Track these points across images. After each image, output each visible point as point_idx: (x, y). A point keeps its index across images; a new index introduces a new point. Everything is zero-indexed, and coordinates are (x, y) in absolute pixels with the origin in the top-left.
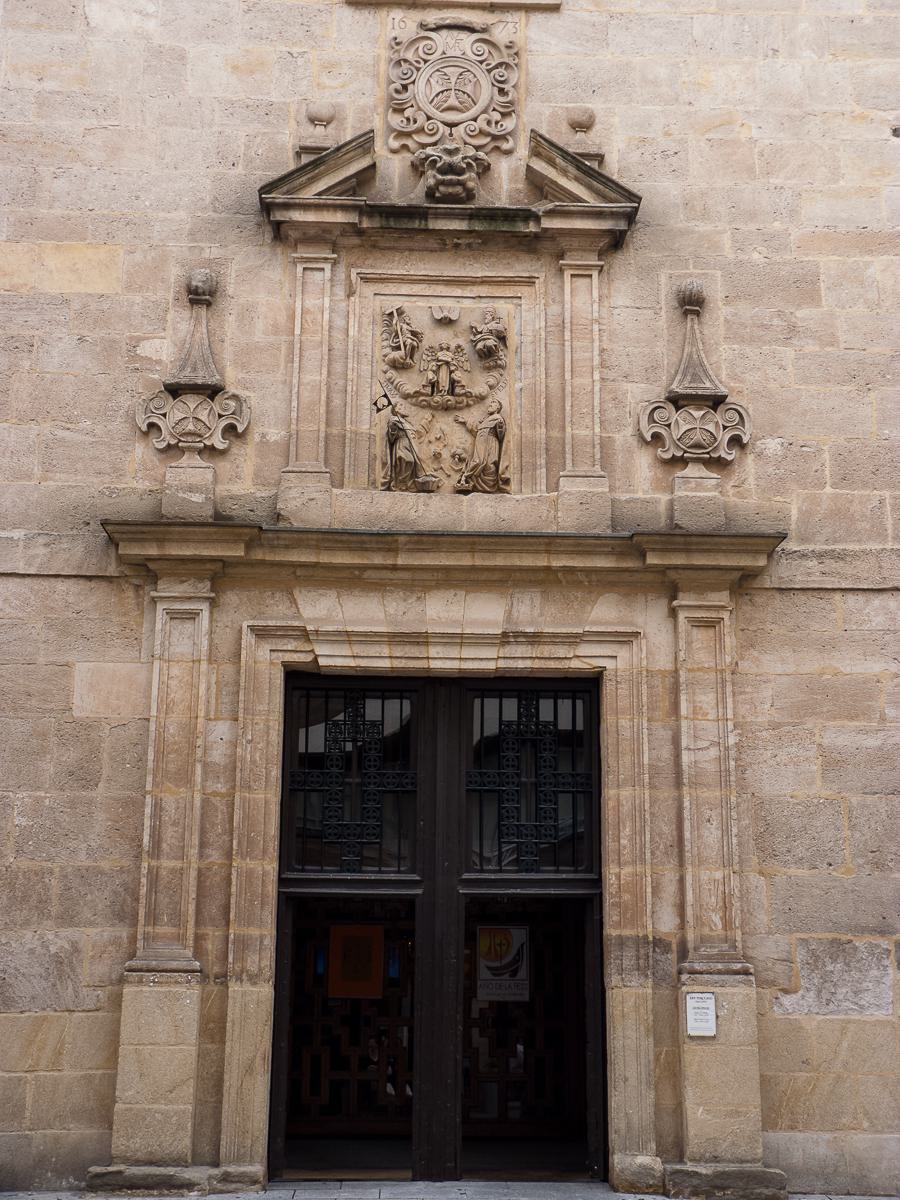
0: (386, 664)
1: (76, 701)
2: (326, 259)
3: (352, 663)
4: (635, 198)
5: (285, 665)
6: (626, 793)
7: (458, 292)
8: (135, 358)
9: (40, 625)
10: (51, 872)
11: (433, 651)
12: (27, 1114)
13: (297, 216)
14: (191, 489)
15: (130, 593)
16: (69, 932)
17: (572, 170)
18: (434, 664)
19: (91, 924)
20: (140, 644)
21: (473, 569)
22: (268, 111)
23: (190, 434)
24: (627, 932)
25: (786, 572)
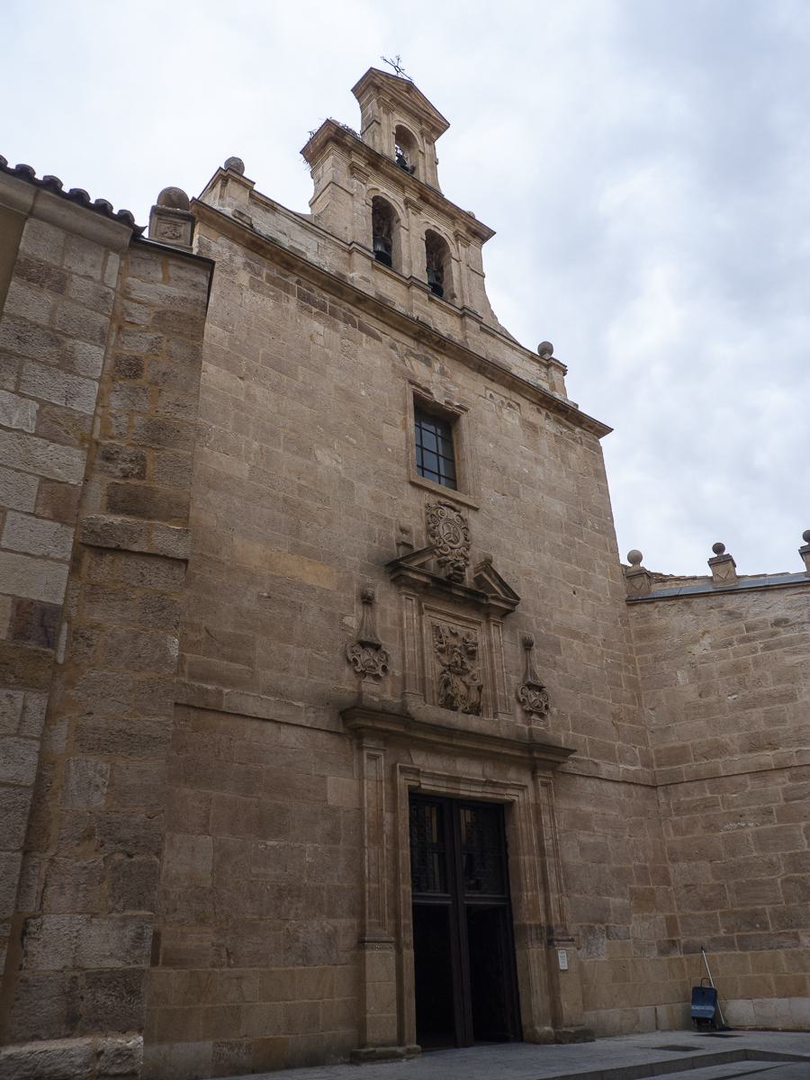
0: (444, 790)
1: (329, 796)
2: (414, 596)
3: (433, 788)
4: (518, 599)
5: (409, 786)
6: (527, 858)
7: (456, 622)
8: (343, 624)
9: (312, 755)
10: (323, 888)
11: (462, 786)
12: (321, 1023)
13: (411, 575)
14: (373, 694)
15: (348, 743)
16: (332, 921)
17: (497, 581)
18: (461, 792)
19: (342, 917)
20: (353, 767)
21: (477, 750)
22: (386, 521)
23: (371, 667)
24: (533, 923)
25: (569, 766)
